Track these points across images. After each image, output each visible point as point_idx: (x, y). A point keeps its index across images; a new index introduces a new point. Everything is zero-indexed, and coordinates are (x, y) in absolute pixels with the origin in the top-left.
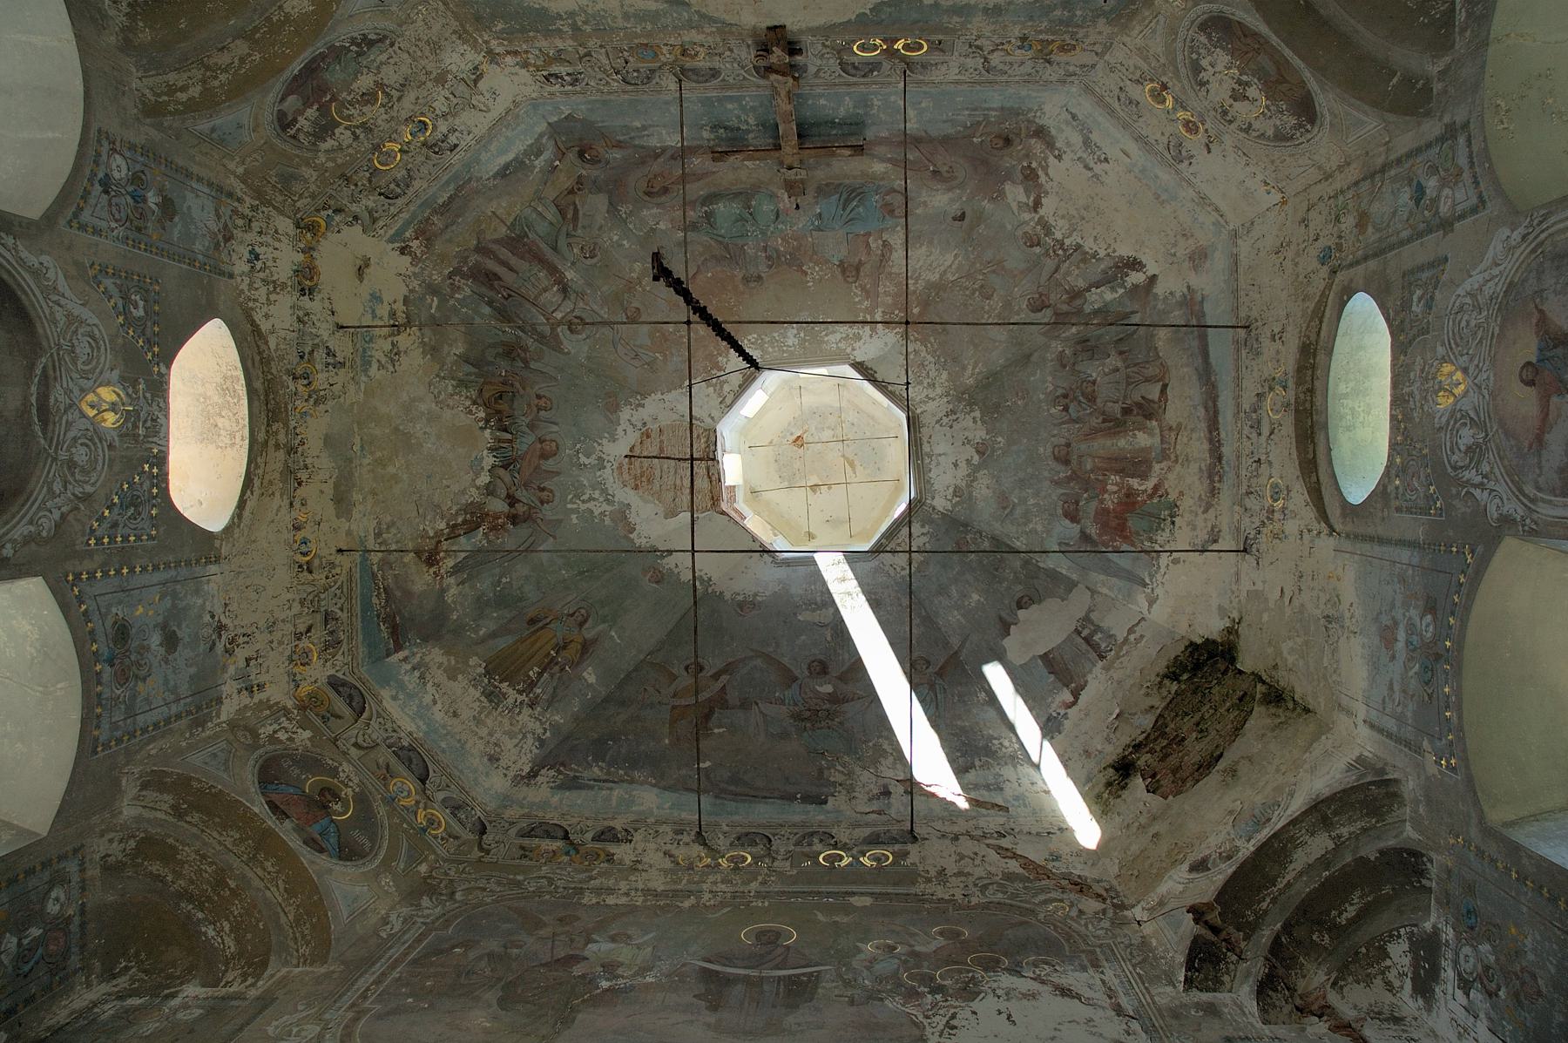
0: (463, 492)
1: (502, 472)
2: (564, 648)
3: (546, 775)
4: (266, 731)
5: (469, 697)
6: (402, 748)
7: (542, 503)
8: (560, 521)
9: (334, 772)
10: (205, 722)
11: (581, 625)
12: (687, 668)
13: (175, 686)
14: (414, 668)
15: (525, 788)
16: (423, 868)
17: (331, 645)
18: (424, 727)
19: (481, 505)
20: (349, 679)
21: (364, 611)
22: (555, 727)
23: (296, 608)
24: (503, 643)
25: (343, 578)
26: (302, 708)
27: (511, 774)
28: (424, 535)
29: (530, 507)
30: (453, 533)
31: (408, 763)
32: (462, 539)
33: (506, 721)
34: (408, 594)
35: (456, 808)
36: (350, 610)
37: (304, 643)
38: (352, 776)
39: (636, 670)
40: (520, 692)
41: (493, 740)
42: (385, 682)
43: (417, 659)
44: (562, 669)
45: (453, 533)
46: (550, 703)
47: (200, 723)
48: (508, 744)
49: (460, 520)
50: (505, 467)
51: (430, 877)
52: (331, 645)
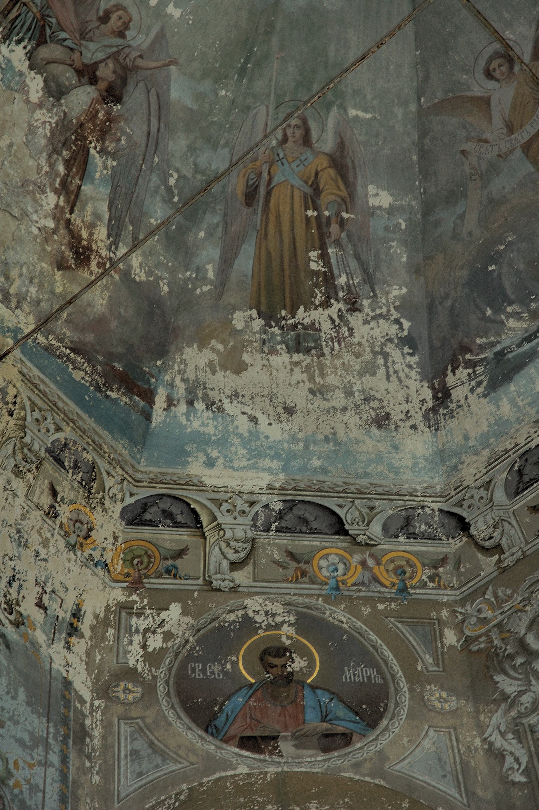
0: (31, 130)
1: (45, 52)
2: (317, 191)
3: (458, 380)
4: (134, 657)
5: (276, 371)
6: (281, 515)
7: (121, 34)
8: (161, 35)
9: (248, 624)
10: (83, 726)
11: (306, 141)
12: (489, 74)
13: (31, 734)
14: (190, 403)
15: (452, 424)
16: (450, 637)
17: (90, 479)
18: (276, 464)
19: (64, 124)
20: (143, 493)
21: (80, 402)
22: (405, 307)
23: (19, 485)
24: (245, 262)
25: (25, 394)
26: (136, 585)
27: (418, 419)
28: (47, 235)
29: (115, 57)
30: (72, 196)
31: (304, 526)
32: (86, 189)
33: (348, 358)
34: (99, 324)
35: (405, 525)
36: (68, 420)
37: (65, 512)
38: (269, 607)
39: (423, 134)
40: (326, 304)
41: (358, 397)
42: (180, 455)
43: (181, 389)
44: (342, 223)
45: (72, 196)
46: (369, 280)
47: (82, 734)
48: (377, 383)
49: (61, 169)
50: (42, 41)
51: (469, 641)
52: (90, 479)
